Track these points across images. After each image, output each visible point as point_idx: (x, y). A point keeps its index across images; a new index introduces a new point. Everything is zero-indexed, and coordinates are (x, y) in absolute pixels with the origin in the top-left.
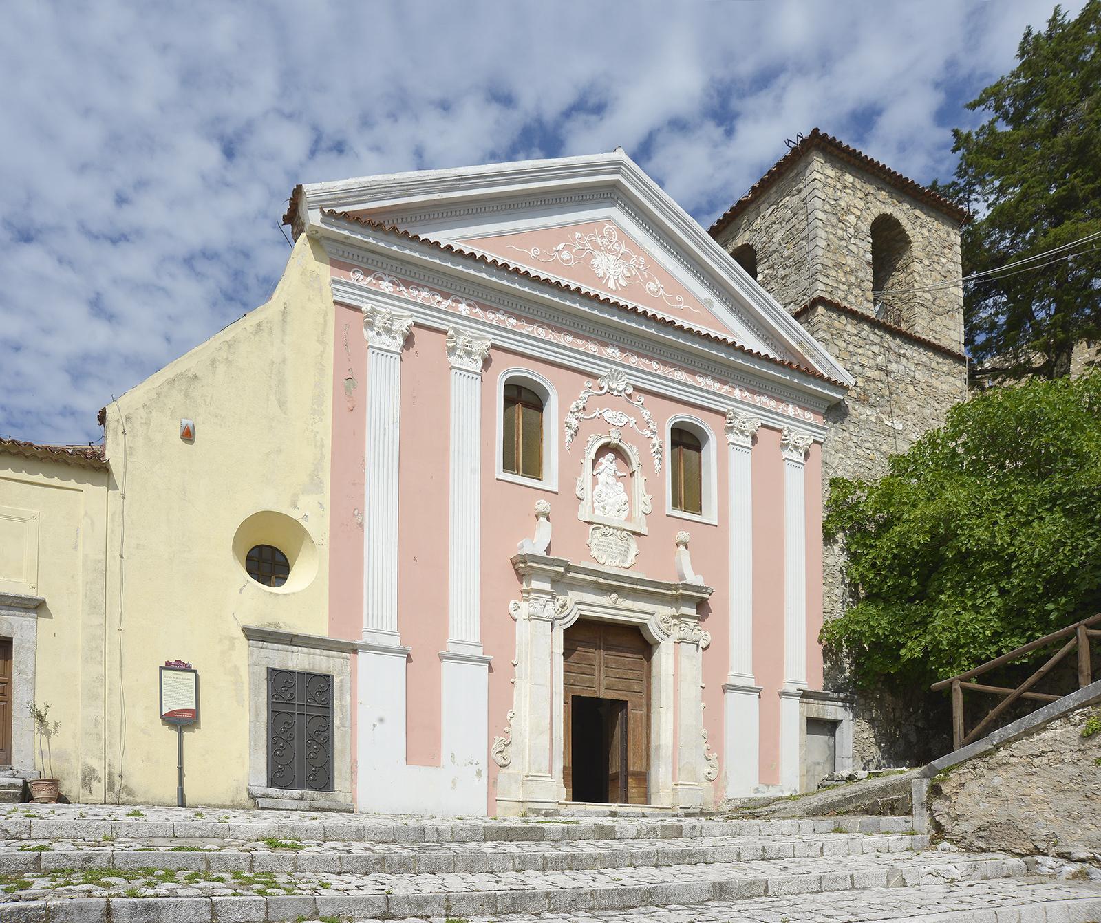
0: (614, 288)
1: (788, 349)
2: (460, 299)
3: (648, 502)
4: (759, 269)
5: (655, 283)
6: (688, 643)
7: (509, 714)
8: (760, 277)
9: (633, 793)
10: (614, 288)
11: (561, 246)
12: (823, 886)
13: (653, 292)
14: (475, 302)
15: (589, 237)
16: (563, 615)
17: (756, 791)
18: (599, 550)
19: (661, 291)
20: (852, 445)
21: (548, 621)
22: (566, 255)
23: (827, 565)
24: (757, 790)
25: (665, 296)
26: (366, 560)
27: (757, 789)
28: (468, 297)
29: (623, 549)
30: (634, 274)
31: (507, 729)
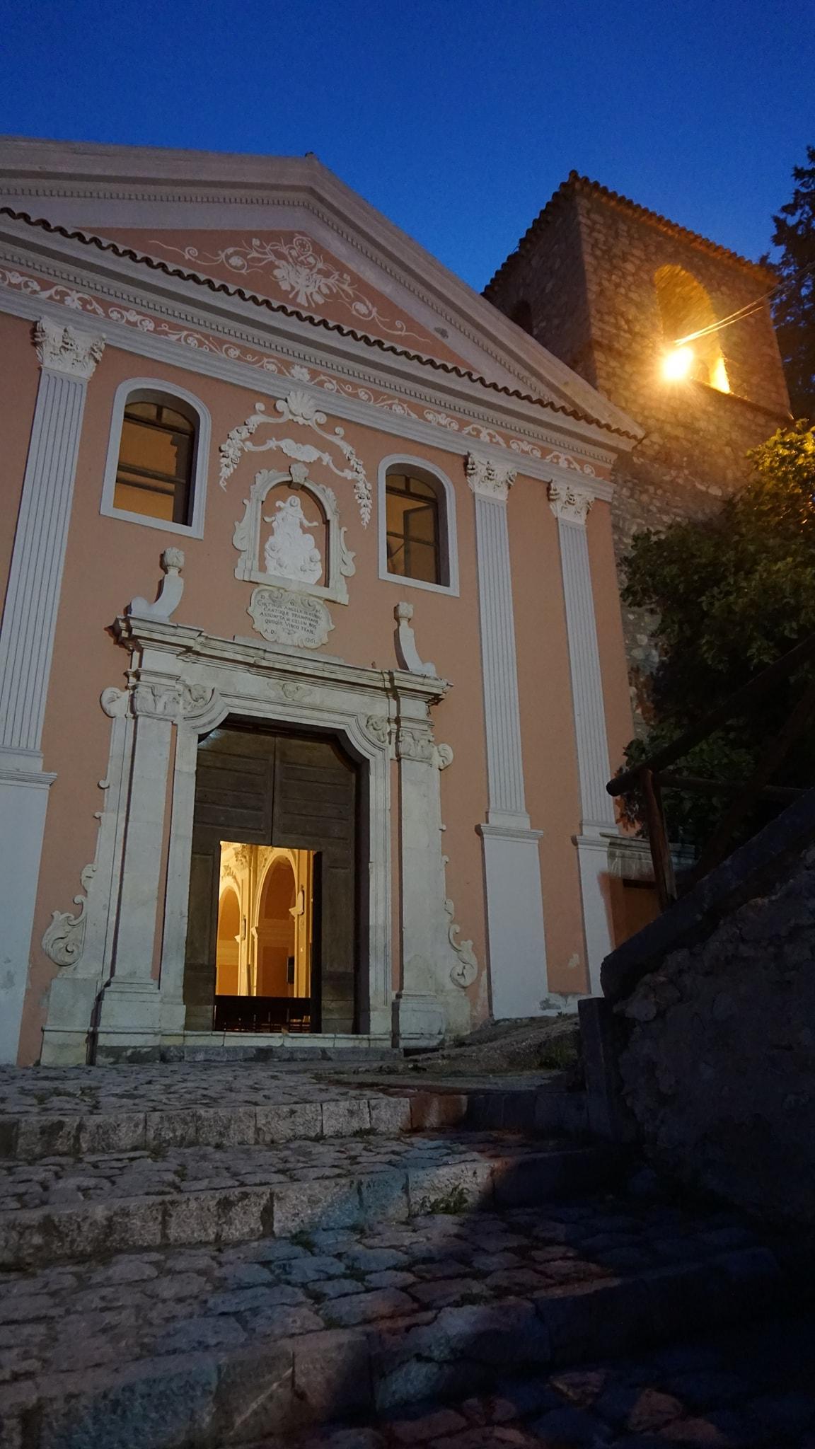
0: (306, 305)
1: (573, 403)
2: (70, 292)
3: (349, 562)
4: (534, 323)
5: (365, 304)
6: (413, 760)
7: (86, 872)
8: (535, 332)
9: (330, 1011)
10: (306, 305)
11: (230, 250)
12: (173, 1232)
13: (364, 315)
14: (92, 296)
15: (273, 246)
16: (197, 713)
17: (545, 1005)
18: (268, 622)
19: (374, 313)
20: (655, 510)
21: (167, 720)
22: (236, 261)
23: (633, 659)
24: (546, 1005)
25: (381, 322)
26: (247, 713)
27: (547, 1001)
28: (80, 288)
29: (308, 622)
30: (335, 291)
31: (78, 899)
